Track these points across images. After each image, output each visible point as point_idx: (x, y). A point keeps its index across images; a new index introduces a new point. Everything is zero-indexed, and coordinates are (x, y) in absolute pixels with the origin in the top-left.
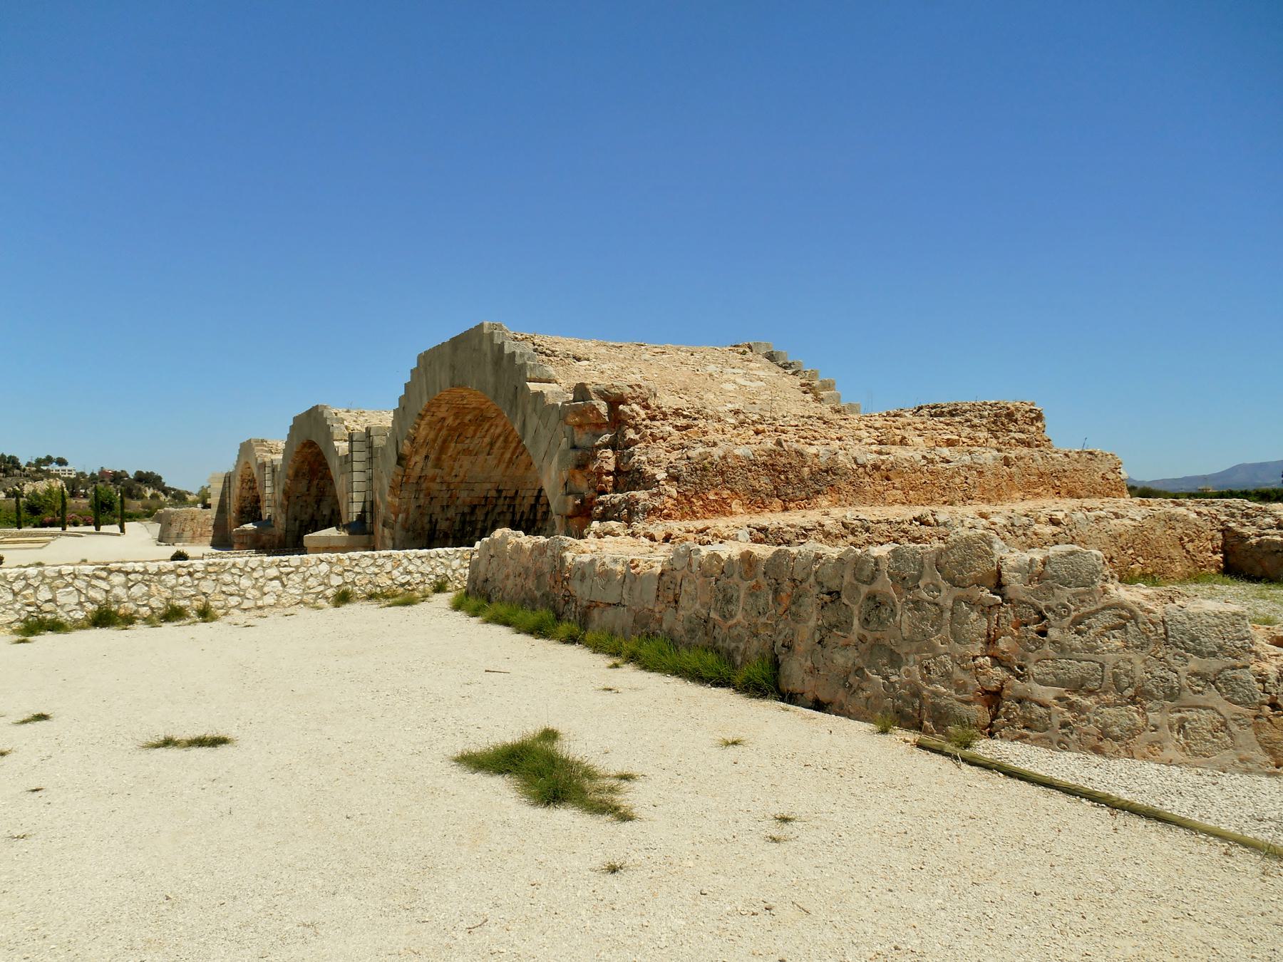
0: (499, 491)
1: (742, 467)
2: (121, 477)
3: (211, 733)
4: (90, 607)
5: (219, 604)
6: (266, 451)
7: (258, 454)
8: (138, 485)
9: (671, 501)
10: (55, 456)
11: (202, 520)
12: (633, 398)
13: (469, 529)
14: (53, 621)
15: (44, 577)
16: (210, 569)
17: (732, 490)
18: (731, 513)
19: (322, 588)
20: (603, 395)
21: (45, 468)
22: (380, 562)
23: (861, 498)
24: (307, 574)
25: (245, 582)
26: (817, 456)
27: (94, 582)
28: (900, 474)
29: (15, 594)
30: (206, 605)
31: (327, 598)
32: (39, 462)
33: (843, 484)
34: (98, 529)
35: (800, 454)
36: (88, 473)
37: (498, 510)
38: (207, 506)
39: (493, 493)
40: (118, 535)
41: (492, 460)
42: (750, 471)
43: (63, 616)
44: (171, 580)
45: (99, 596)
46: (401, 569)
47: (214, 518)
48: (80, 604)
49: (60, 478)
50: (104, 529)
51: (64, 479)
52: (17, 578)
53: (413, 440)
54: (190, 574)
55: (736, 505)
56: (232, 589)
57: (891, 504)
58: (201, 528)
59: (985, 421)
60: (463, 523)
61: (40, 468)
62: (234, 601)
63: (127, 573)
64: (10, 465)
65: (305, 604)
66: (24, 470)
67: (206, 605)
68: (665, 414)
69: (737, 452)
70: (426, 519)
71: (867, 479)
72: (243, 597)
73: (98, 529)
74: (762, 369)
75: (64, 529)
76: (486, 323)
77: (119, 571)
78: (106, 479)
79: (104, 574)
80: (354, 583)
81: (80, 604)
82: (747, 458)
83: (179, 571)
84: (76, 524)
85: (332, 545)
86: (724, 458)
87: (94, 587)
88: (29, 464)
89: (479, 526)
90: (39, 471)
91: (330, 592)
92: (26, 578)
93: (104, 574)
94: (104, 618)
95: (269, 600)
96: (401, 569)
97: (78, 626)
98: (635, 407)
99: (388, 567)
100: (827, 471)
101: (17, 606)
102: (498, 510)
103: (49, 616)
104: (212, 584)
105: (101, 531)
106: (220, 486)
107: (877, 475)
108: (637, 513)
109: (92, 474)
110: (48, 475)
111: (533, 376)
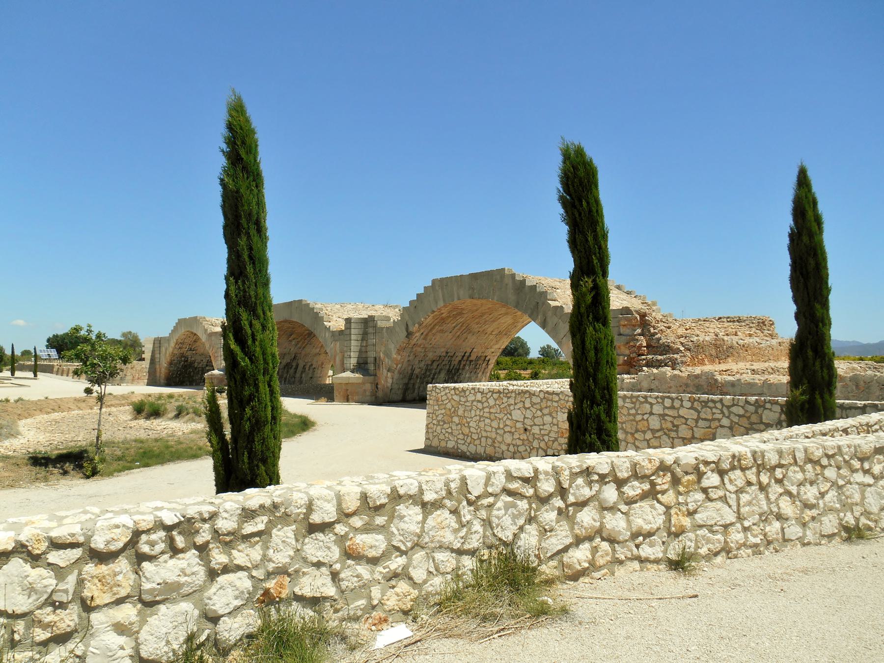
0: (447, 353)
6: (210, 325)
13: (428, 373)
20: (638, 312)
33: (735, 353)
37: (444, 363)
39: (444, 354)
40: (31, 379)
41: (450, 336)
50: (18, 374)
58: (139, 374)
59: (754, 325)
60: (426, 370)
70: (410, 367)
76: (506, 268)
85: (350, 382)
86: (703, 341)
89: (433, 372)
102: (444, 363)
105: (15, 376)
106: (151, 346)
108: (678, 364)
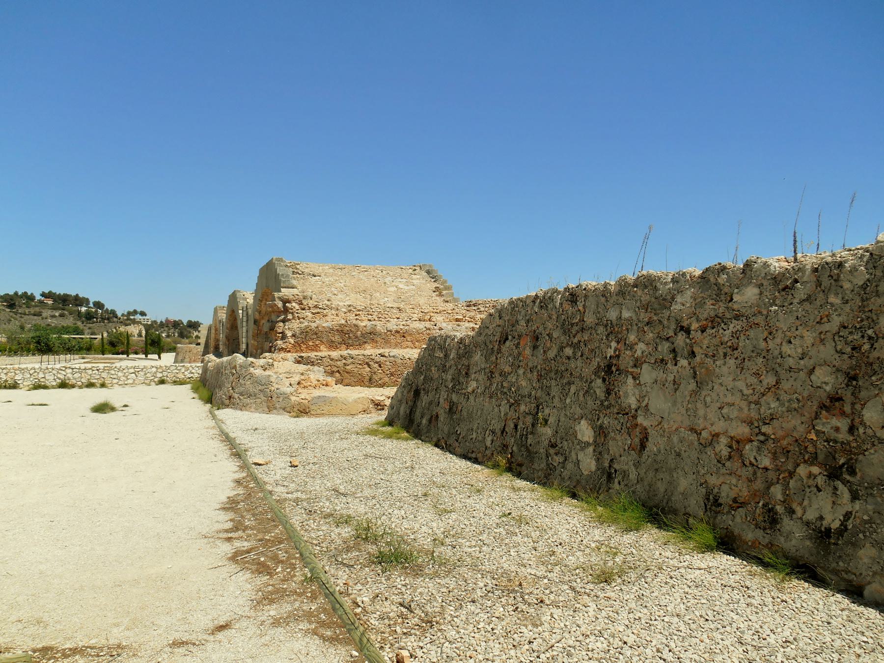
1: (326, 331)
2: (179, 324)
3: (44, 403)
4: (58, 381)
5: (109, 382)
7: (219, 315)
8: (189, 329)
9: (291, 345)
10: (139, 310)
11: (195, 352)
12: (294, 300)
14: (44, 385)
15: (41, 369)
16: (106, 368)
17: (321, 341)
18: (320, 351)
19: (153, 378)
21: (132, 317)
22: (179, 368)
23: (389, 345)
24: (147, 372)
25: (120, 374)
26: (365, 327)
27: (60, 371)
28: (411, 335)
29: (31, 375)
30: (104, 382)
31: (155, 382)
32: (129, 313)
33: (378, 339)
34: (146, 356)
35: (355, 325)
36: (159, 321)
38: (198, 344)
40: (157, 360)
42: (330, 333)
43: (48, 384)
44: (90, 372)
45: (62, 377)
46: (189, 371)
47: (202, 350)
48: (54, 379)
49: (141, 324)
50: (150, 356)
51: (144, 325)
52: (31, 369)
53: (260, 312)
54: (98, 370)
55: (322, 347)
56: (115, 376)
57: (404, 348)
61: (129, 318)
62: (115, 381)
63: (73, 369)
64: (112, 315)
65: (146, 384)
66: (120, 318)
67: (104, 382)
68: (310, 308)
69: (324, 325)
71: (392, 337)
72: (119, 380)
73: (146, 356)
74: (420, 279)
75: (128, 356)
76: (274, 258)
77: (70, 368)
78: (170, 325)
79: (64, 369)
80: (167, 376)
81: (54, 379)
82: (328, 327)
83: (93, 369)
84: (136, 353)
86: (317, 327)
87: (60, 373)
88: (123, 315)
90: (128, 319)
91: (156, 380)
92: (34, 369)
93: (64, 369)
94: (63, 385)
95: (130, 381)
96: (189, 371)
97: (53, 387)
98: (294, 304)
99: (183, 370)
100: (370, 334)
101: (31, 379)
103: (43, 384)
104: (107, 374)
107: (398, 335)
109: (161, 322)
110: (134, 322)
111: (285, 285)
